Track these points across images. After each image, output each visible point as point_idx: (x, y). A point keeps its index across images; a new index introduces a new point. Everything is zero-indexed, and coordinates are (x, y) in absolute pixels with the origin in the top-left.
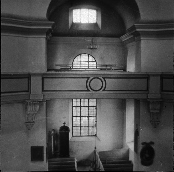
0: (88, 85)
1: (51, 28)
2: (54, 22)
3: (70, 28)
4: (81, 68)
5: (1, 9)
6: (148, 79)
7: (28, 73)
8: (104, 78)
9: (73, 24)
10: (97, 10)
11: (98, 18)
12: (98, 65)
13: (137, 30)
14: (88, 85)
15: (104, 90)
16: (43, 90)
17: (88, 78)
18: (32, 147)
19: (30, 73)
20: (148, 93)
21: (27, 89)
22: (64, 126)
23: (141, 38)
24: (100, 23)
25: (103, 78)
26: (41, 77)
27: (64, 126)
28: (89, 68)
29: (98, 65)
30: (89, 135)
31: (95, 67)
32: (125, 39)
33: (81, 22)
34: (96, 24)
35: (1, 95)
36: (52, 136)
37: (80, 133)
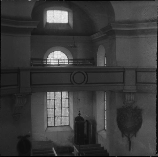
0: (72, 78)
1: (36, 27)
2: (39, 22)
3: (45, 26)
4: (62, 63)
5: (1, 8)
6: (124, 72)
7: (122, 67)
8: (86, 72)
9: (47, 24)
10: (69, 12)
11: (70, 18)
12: (70, 59)
13: (113, 29)
14: (72, 78)
15: (86, 84)
16: (31, 85)
17: (72, 73)
18: (19, 137)
19: (124, 67)
20: (125, 85)
21: (122, 82)
22: (79, 116)
23: (116, 37)
24: (71, 23)
25: (85, 72)
26: (134, 71)
27: (79, 116)
28: (77, 62)
29: (70, 59)
30: (55, 125)
31: (57, 62)
32: (97, 38)
33: (62, 22)
34: (68, 24)
35: (1, 88)
36: (91, 125)
37: (55, 123)
